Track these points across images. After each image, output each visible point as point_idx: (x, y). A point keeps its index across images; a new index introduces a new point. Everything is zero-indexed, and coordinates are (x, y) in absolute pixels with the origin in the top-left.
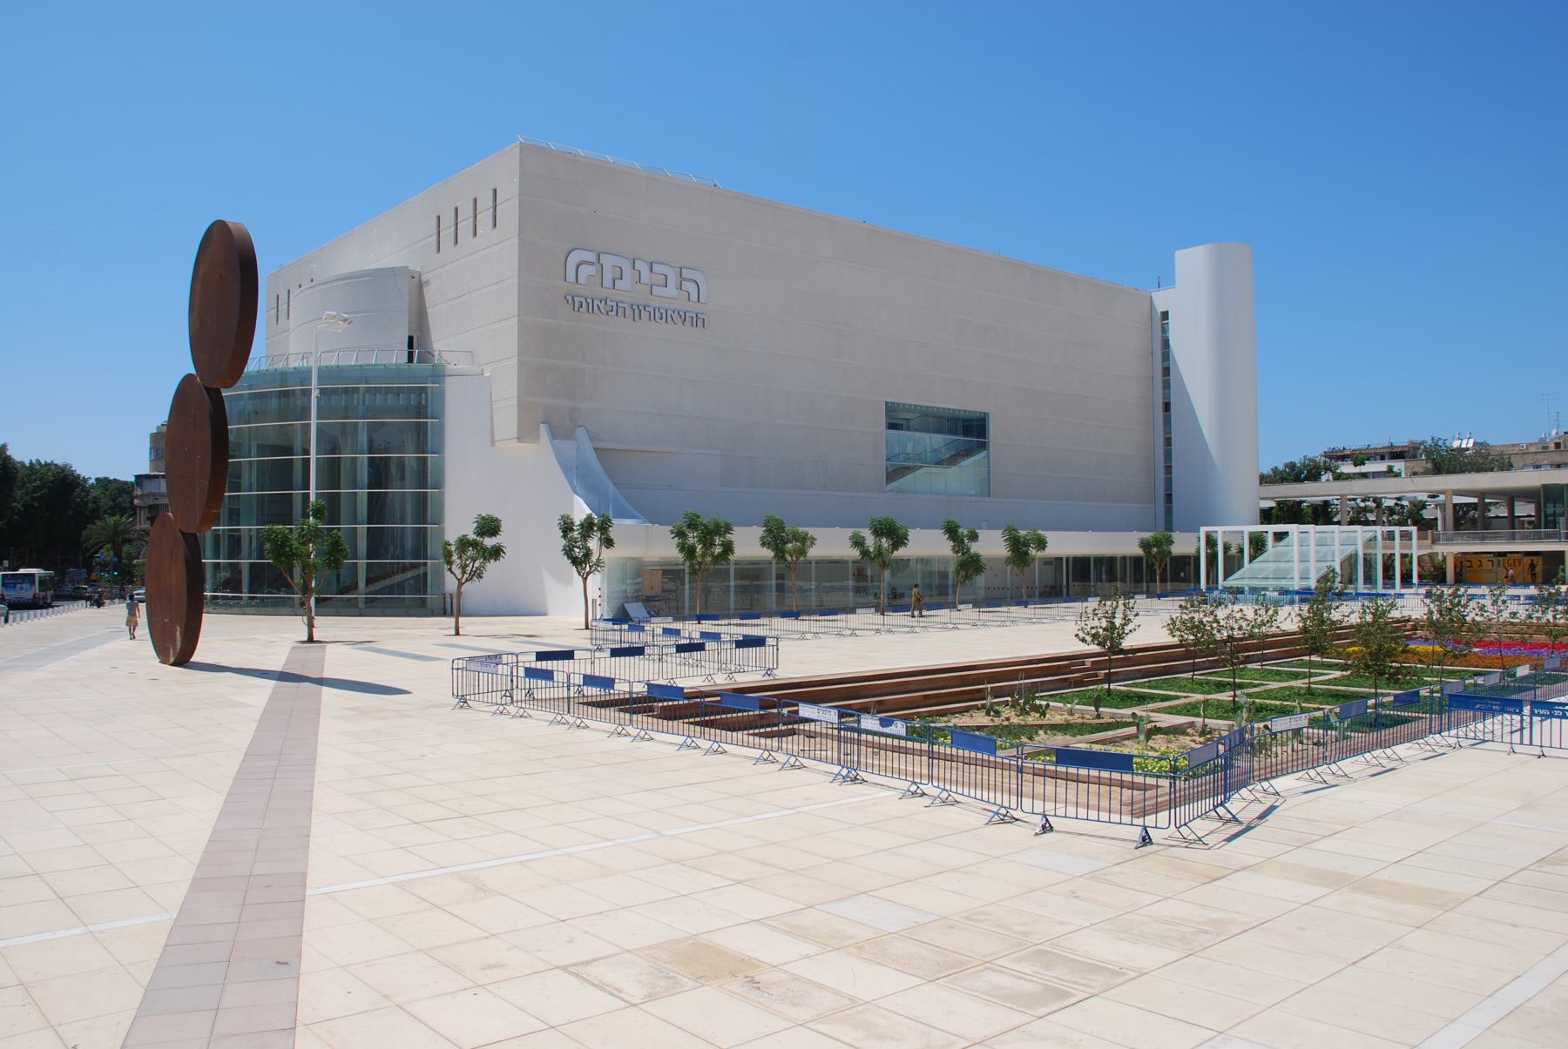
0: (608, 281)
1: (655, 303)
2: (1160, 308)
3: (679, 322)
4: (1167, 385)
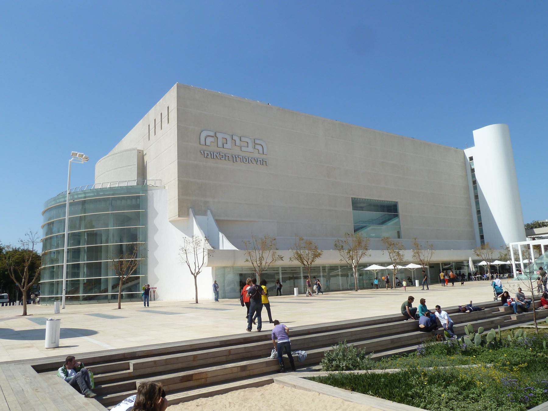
0: (220, 144)
1: (243, 154)
2: (468, 156)
3: (255, 163)
4: (477, 203)
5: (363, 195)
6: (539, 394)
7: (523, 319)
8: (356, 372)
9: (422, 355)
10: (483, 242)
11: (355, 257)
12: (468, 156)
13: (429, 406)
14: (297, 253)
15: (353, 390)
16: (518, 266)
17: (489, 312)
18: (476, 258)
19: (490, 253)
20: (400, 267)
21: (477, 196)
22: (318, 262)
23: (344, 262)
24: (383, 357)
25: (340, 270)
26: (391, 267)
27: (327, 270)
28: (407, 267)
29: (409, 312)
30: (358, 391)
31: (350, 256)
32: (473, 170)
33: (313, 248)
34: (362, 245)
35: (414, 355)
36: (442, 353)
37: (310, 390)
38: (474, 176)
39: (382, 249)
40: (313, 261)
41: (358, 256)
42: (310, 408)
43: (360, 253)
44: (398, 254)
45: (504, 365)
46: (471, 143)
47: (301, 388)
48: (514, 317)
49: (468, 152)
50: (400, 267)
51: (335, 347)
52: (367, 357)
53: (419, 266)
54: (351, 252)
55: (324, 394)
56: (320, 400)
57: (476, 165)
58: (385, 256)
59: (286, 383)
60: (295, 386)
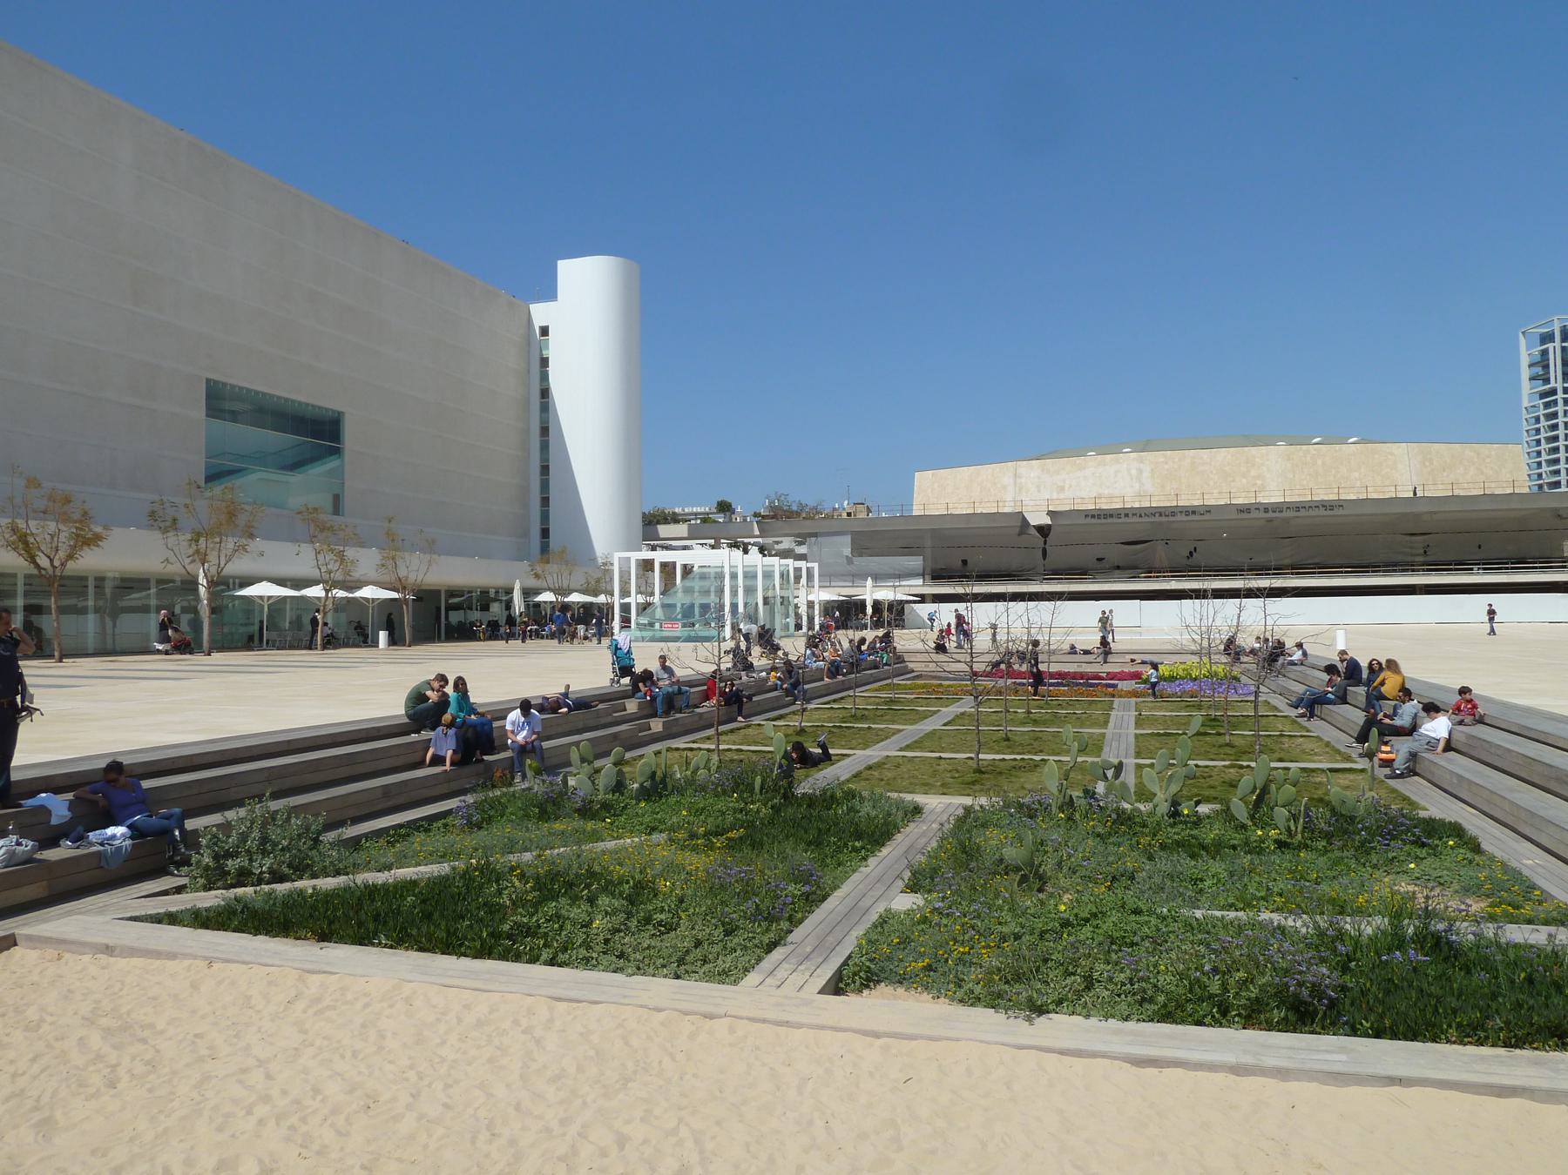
2: (538, 323)
4: (545, 447)
5: (243, 377)
6: (794, 896)
7: (675, 730)
8: (306, 884)
9: (473, 826)
10: (545, 548)
11: (213, 557)
12: (538, 323)
13: (561, 957)
14: (14, 530)
15: (324, 937)
16: (626, 608)
17: (608, 712)
18: (532, 583)
19: (566, 574)
20: (341, 594)
21: (547, 429)
22: (90, 561)
23: (174, 569)
24: (368, 836)
25: (153, 591)
26: (316, 592)
27: (108, 591)
28: (359, 594)
29: (426, 711)
30: (342, 940)
31: (198, 552)
32: (544, 362)
33: (76, 516)
34: (236, 523)
35: (445, 825)
36: (527, 816)
37: (172, 956)
38: (544, 377)
39: (295, 540)
40: (70, 557)
41: (223, 552)
42: (194, 1012)
43: (231, 546)
44: (341, 557)
45: (693, 836)
46: (548, 292)
47: (132, 952)
48: (657, 725)
49: (540, 313)
50: (341, 594)
51: (231, 815)
52: (330, 836)
53: (394, 595)
54: (202, 540)
55: (228, 961)
56: (220, 983)
57: (555, 350)
58: (302, 560)
59: (73, 942)
60: (108, 950)
